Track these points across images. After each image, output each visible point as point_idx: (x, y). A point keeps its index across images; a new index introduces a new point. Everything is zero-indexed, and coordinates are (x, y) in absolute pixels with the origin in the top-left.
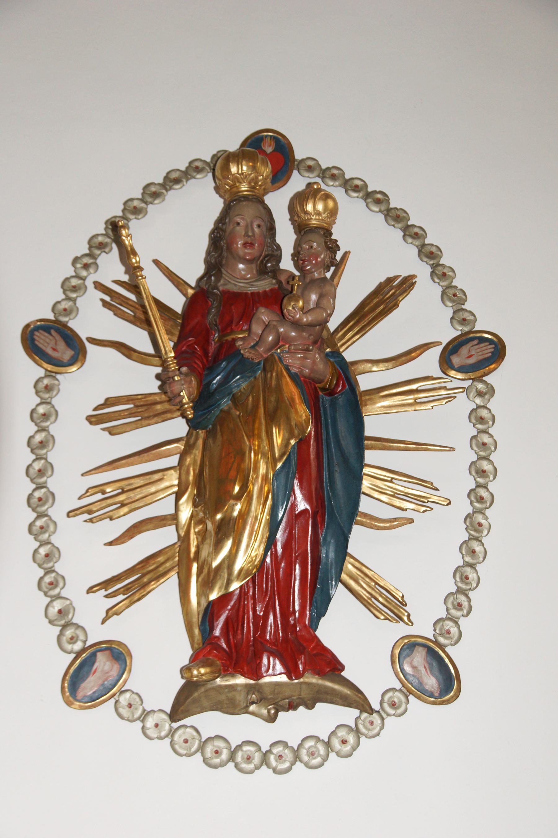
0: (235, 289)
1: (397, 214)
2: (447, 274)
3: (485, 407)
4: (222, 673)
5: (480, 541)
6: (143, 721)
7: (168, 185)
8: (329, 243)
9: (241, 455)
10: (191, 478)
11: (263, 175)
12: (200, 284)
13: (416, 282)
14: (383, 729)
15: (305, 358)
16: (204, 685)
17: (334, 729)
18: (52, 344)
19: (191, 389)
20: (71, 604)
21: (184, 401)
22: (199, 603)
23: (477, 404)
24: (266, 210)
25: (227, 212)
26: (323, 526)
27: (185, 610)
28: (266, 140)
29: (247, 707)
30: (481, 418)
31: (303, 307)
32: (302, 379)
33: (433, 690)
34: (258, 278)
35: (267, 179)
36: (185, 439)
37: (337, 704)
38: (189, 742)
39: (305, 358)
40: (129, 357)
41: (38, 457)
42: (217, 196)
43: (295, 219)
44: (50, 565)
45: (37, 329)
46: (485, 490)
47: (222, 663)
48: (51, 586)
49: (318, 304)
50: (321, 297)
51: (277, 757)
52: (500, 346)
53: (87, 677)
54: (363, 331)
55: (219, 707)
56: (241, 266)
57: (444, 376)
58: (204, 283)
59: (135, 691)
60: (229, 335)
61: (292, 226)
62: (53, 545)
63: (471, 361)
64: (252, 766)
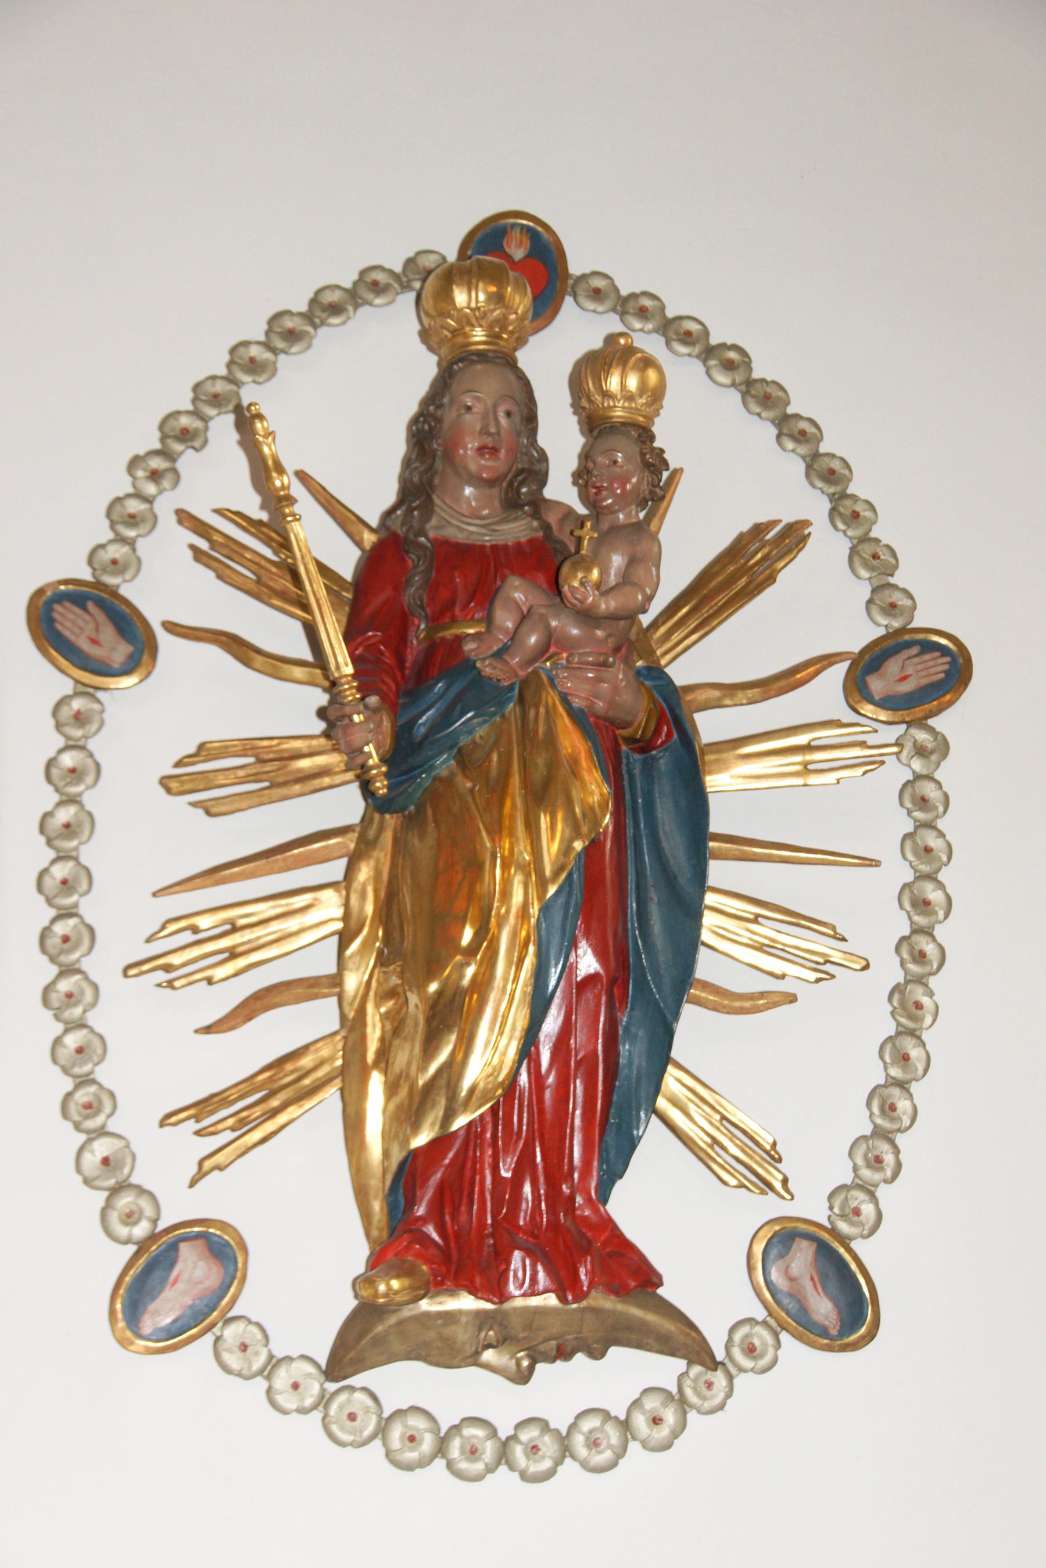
0: (460, 537)
1: (765, 392)
2: (862, 514)
3: (929, 778)
4: (432, 1289)
5: (919, 1038)
6: (268, 1378)
7: (319, 317)
8: (648, 456)
9: (476, 868)
10: (369, 909)
11: (516, 313)
12: (389, 523)
13: (810, 534)
14: (731, 1396)
15: (598, 680)
16: (395, 1311)
17: (638, 1396)
18: (90, 630)
19: (380, 737)
20: (128, 1146)
21: (371, 762)
22: (386, 1154)
23: (914, 772)
24: (522, 382)
25: (445, 383)
26: (624, 1006)
27: (354, 1161)
28: (511, 232)
29: (477, 1353)
30: (924, 799)
31: (601, 582)
32: (592, 719)
33: (827, 1323)
34: (505, 515)
35: (525, 319)
36: (358, 829)
37: (649, 1350)
38: (359, 1418)
39: (598, 680)
40: (247, 663)
41: (62, 854)
42: (423, 348)
43: (582, 405)
44: (87, 1068)
45: (60, 598)
46: (929, 939)
47: (432, 1269)
48: (88, 1111)
49: (626, 579)
50: (633, 561)
51: (529, 1449)
52: (961, 661)
53: (160, 1292)
54: (706, 625)
55: (423, 1353)
56: (468, 491)
57: (853, 718)
58: (399, 522)
59: (254, 1319)
60: (448, 629)
61: (575, 419)
62: (92, 1030)
63: (907, 687)
64: (480, 1466)
